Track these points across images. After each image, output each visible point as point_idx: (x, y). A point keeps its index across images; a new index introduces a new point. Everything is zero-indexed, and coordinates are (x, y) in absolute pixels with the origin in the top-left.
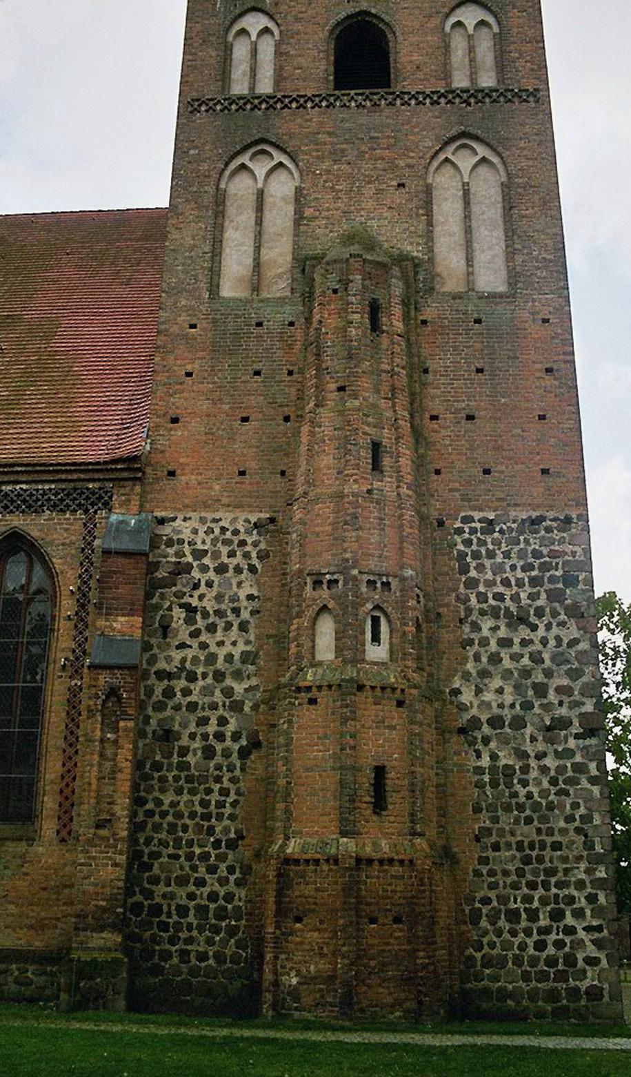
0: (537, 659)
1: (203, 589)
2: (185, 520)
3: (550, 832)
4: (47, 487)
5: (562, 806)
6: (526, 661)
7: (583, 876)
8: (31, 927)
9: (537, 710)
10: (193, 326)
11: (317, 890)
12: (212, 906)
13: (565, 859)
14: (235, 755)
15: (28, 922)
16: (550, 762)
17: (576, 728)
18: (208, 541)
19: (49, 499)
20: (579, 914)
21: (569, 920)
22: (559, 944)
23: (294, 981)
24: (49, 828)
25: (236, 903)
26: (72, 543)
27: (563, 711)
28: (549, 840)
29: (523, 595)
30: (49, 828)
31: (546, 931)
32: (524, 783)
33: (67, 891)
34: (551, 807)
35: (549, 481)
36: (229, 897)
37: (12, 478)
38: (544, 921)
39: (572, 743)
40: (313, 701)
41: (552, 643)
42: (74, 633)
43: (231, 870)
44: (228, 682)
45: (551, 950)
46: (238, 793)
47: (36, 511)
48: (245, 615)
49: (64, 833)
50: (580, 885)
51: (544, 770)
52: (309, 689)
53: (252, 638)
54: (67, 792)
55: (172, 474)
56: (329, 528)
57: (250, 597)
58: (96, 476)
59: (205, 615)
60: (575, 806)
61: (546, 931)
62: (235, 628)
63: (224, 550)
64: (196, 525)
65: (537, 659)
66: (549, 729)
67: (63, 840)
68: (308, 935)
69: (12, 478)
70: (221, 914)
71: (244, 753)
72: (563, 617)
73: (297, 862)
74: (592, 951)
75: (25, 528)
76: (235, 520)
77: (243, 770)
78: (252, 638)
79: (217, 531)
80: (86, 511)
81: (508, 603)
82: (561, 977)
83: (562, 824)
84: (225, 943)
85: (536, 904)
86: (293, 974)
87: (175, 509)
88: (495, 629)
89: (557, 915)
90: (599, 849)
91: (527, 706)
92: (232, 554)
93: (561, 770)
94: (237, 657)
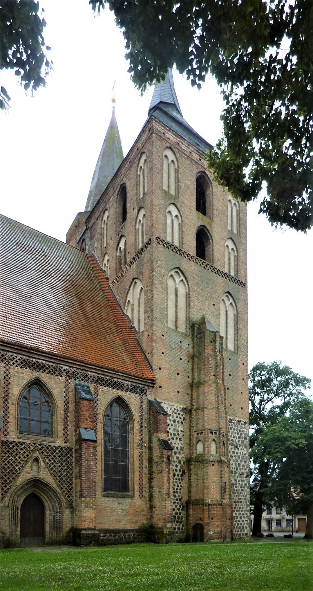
0: (239, 458)
1: (170, 426)
2: (165, 403)
3: (240, 499)
4: (32, 359)
5: (242, 493)
6: (237, 457)
7: (245, 509)
8: (134, 523)
9: (239, 470)
10: (163, 336)
11: (217, 512)
12: (177, 516)
13: (242, 505)
14: (180, 476)
15: (133, 521)
16: (240, 482)
17: (245, 475)
18: (171, 412)
19: (129, 387)
20: (244, 517)
21: (243, 519)
22: (241, 524)
23: (212, 533)
24: (137, 494)
25: (182, 515)
26: (137, 405)
27: (243, 471)
28: (240, 501)
29: (237, 441)
30: (137, 494)
31: (239, 521)
32: (236, 487)
33: (143, 512)
34: (240, 493)
35: (242, 411)
36: (180, 514)
37: (118, 377)
38: (239, 519)
39: (244, 479)
40: (213, 465)
41: (242, 453)
42: (139, 435)
43: (180, 506)
44: (177, 455)
45: (240, 525)
46: (181, 486)
47: (125, 391)
48: (181, 436)
49: (141, 496)
50: (245, 511)
51: (239, 484)
52: (212, 461)
53: (182, 443)
54: (141, 484)
55: (160, 387)
56: (214, 417)
57: (181, 431)
58: (143, 383)
59: (171, 434)
60: (244, 493)
61: (239, 521)
62: (178, 439)
63: (175, 415)
64: (168, 406)
65: (239, 458)
66: (240, 475)
67: (141, 498)
68: (216, 522)
69: (118, 377)
70: (178, 518)
71: (182, 475)
72: (244, 448)
73: (212, 505)
74: (246, 525)
75: (123, 396)
76: (177, 406)
77: (182, 480)
78: (182, 443)
79: (173, 409)
80: (140, 395)
81: (234, 442)
82: (241, 531)
83: (242, 497)
84: (179, 525)
85: (237, 515)
86: (211, 531)
87: (162, 399)
88: (232, 448)
89: (241, 518)
90: (248, 503)
91: (237, 469)
92: (177, 417)
93: (242, 484)
94: (179, 448)
